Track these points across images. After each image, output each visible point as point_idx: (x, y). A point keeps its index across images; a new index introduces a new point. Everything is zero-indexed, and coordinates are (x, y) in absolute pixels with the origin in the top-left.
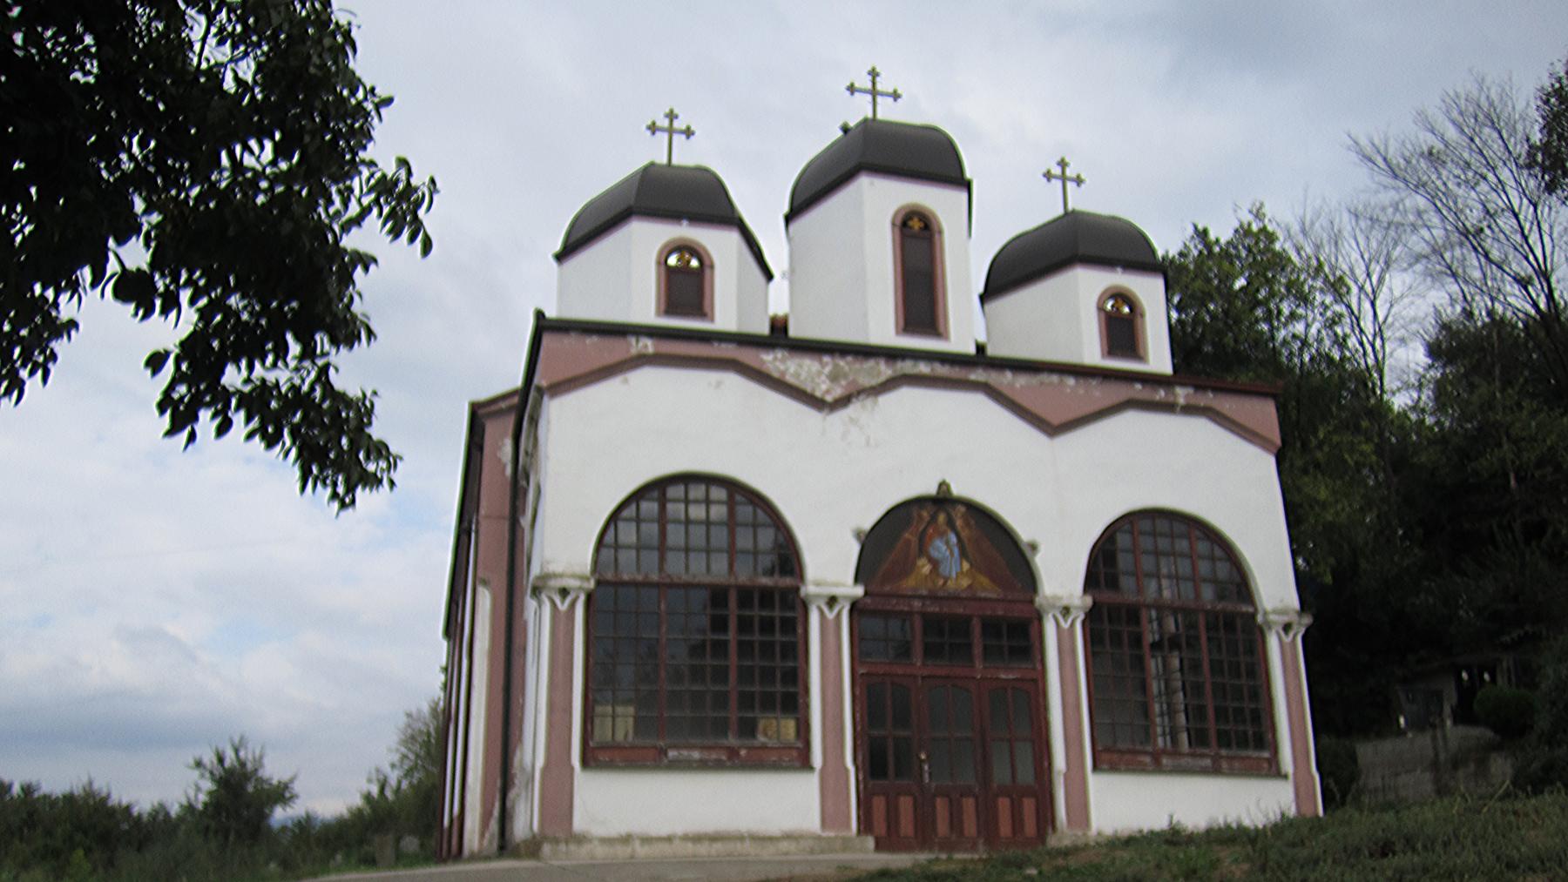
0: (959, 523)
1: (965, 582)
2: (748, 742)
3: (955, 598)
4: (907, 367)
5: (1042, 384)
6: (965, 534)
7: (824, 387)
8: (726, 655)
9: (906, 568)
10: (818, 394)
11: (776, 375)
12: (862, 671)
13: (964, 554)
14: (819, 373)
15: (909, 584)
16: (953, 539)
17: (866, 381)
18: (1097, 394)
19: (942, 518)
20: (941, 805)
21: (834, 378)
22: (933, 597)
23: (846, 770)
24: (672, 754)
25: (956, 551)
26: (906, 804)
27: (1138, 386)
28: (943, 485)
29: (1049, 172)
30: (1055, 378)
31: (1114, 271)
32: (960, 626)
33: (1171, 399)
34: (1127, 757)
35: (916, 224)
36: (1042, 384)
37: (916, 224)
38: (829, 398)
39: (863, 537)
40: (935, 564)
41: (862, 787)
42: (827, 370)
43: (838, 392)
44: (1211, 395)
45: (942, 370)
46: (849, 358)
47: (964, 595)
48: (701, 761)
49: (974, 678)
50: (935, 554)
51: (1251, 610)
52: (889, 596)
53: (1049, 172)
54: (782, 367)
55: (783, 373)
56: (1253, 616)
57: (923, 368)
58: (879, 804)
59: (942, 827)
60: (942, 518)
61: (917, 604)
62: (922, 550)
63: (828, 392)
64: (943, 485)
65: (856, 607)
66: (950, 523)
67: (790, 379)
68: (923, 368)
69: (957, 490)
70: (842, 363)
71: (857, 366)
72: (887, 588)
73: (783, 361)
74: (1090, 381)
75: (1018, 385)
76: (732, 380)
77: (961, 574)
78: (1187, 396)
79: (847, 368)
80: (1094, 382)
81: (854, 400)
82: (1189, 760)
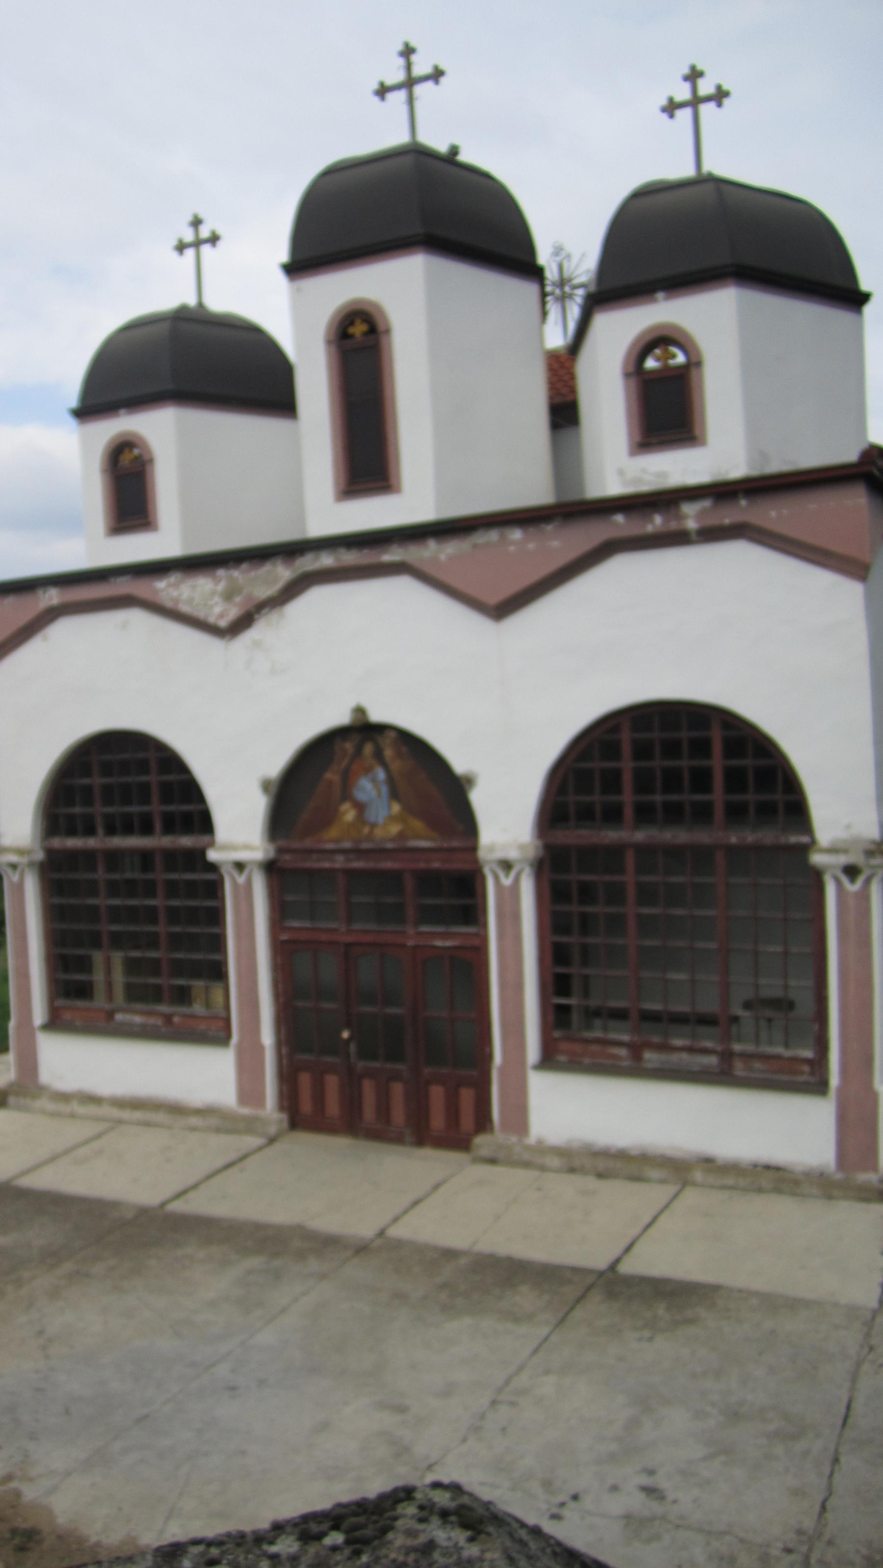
0: (388, 753)
1: (395, 829)
2: (184, 1010)
3: (380, 852)
4: (308, 563)
5: (475, 546)
6: (396, 766)
7: (217, 610)
8: (618, 791)
9: (328, 817)
10: (211, 620)
11: (169, 604)
12: (284, 937)
13: (394, 794)
14: (213, 593)
15: (331, 837)
16: (381, 774)
17: (264, 592)
18: (555, 544)
19: (368, 749)
20: (368, 1088)
21: (228, 596)
22: (358, 852)
23: (261, 1048)
24: (119, 1017)
25: (384, 789)
26: (332, 1082)
27: (619, 518)
28: (360, 711)
29: (701, 74)
30: (493, 535)
31: (655, 301)
32: (392, 880)
33: (673, 525)
34: (595, 1048)
35: (358, 329)
36: (475, 546)
37: (358, 329)
38: (223, 623)
39: (274, 789)
40: (360, 807)
41: (285, 1062)
42: (221, 587)
43: (233, 613)
44: (743, 502)
45: (350, 557)
46: (245, 566)
47: (389, 845)
48: (143, 1026)
49: (403, 946)
50: (361, 796)
51: (804, 839)
52: (309, 852)
53: (701, 74)
54: (175, 594)
55: (177, 601)
56: (804, 850)
57: (326, 560)
58: (305, 1080)
59: (369, 1112)
60: (368, 749)
61: (339, 862)
62: (346, 794)
63: (221, 616)
64: (360, 711)
65: (270, 868)
66: (379, 755)
67: (185, 608)
68: (326, 560)
69: (376, 716)
70: (236, 573)
71: (253, 574)
72: (308, 843)
73: (176, 586)
74: (543, 526)
75: (443, 557)
76: (136, 617)
77: (392, 819)
78: (700, 516)
79: (241, 581)
80: (549, 528)
81: (256, 616)
82: (685, 1056)
